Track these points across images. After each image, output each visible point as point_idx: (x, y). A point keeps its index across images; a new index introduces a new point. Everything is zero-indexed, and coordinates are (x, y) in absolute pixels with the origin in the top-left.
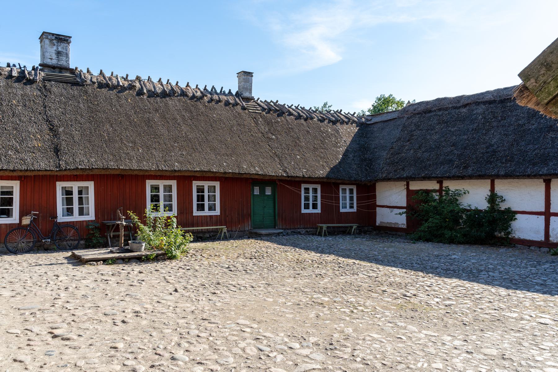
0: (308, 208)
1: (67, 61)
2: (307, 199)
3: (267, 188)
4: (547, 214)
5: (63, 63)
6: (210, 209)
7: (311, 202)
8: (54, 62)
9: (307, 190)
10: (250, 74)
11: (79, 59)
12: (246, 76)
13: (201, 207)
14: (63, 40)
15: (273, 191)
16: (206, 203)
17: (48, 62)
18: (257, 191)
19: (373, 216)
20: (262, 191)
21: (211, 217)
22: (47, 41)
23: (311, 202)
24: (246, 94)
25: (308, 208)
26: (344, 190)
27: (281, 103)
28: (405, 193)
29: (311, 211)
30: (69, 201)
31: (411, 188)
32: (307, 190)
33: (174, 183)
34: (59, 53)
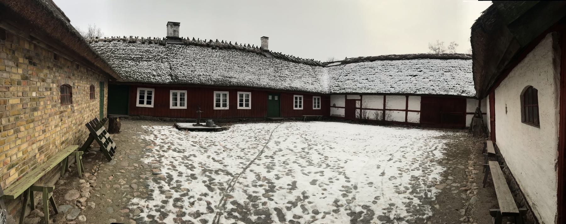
0: (219, 106)
1: (178, 34)
2: (296, 102)
3: (331, 113)
4: (407, 111)
5: (176, 35)
6: (181, 105)
7: (298, 104)
8: (172, 35)
9: (296, 98)
10: (267, 38)
11: (183, 34)
12: (265, 38)
13: (241, 105)
14: (177, 24)
15: (279, 98)
16: (244, 103)
17: (170, 35)
18: (270, 98)
19: (329, 111)
20: (273, 98)
21: (246, 110)
22: (169, 26)
23: (298, 104)
24: (265, 49)
25: (219, 106)
26: (315, 99)
27: (283, 54)
28: (344, 101)
29: (298, 108)
30: (175, 99)
31: (348, 98)
32: (296, 98)
33: (227, 93)
34: (175, 31)
